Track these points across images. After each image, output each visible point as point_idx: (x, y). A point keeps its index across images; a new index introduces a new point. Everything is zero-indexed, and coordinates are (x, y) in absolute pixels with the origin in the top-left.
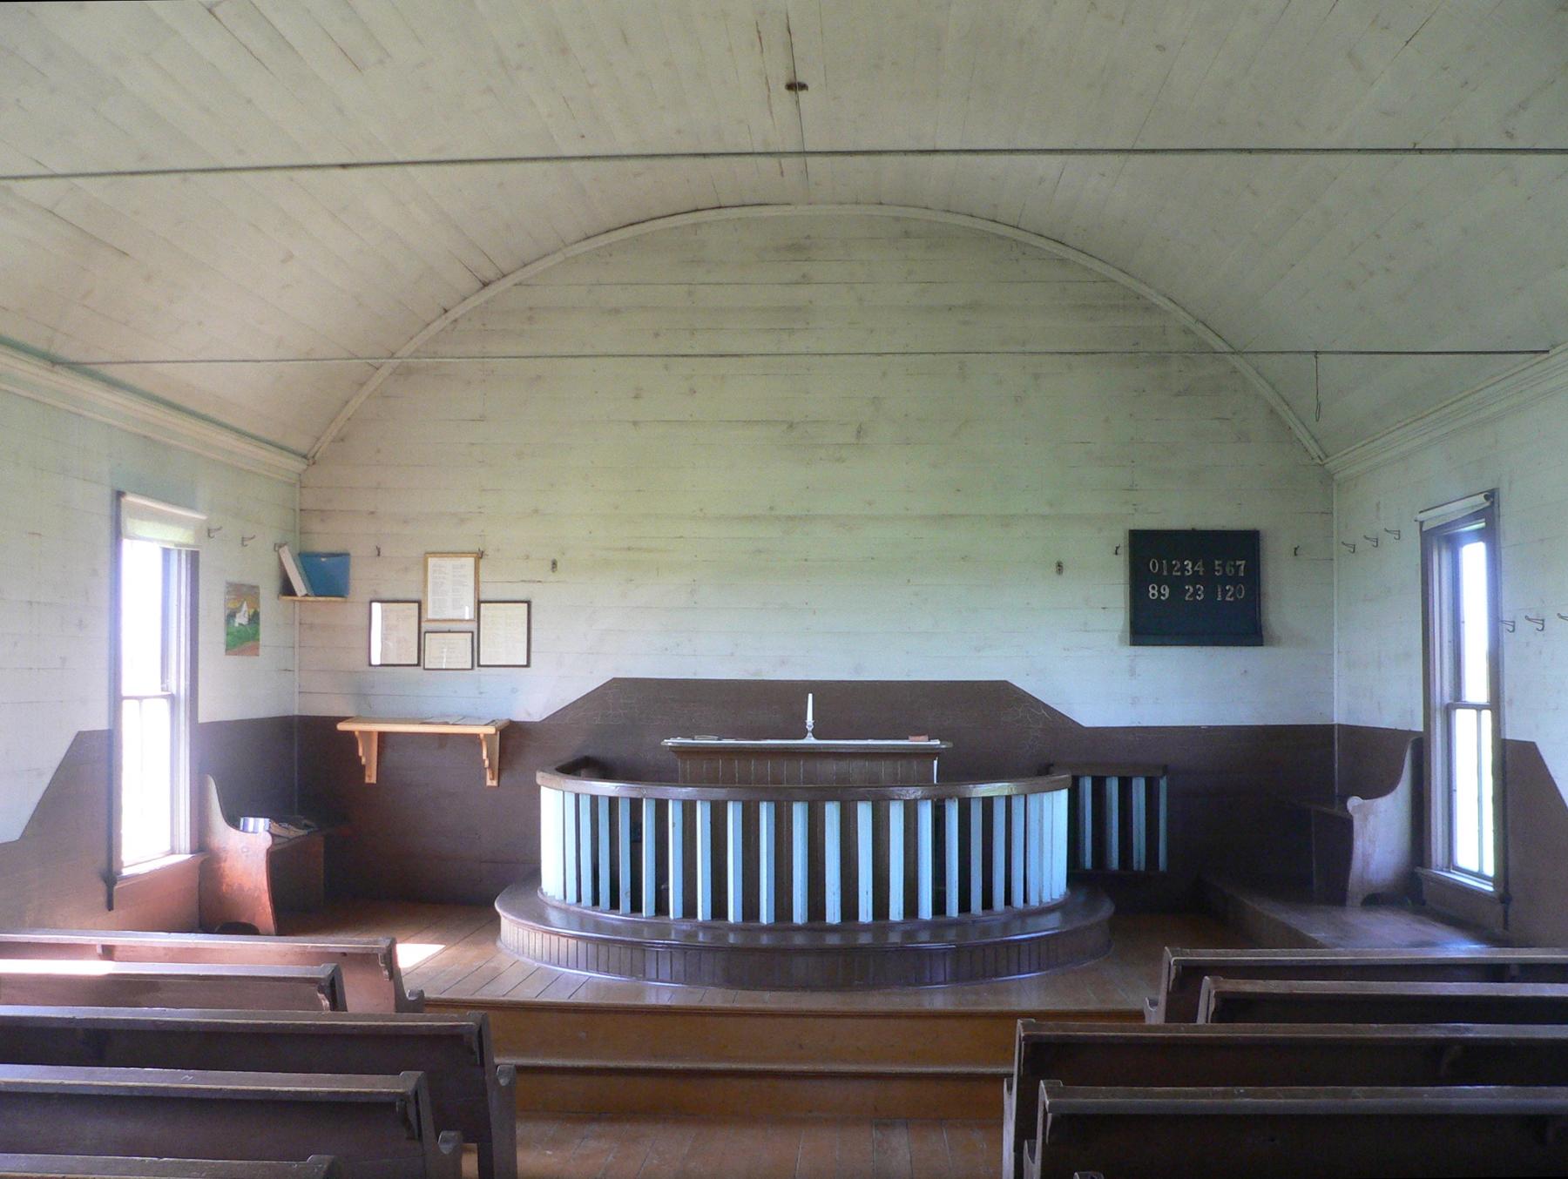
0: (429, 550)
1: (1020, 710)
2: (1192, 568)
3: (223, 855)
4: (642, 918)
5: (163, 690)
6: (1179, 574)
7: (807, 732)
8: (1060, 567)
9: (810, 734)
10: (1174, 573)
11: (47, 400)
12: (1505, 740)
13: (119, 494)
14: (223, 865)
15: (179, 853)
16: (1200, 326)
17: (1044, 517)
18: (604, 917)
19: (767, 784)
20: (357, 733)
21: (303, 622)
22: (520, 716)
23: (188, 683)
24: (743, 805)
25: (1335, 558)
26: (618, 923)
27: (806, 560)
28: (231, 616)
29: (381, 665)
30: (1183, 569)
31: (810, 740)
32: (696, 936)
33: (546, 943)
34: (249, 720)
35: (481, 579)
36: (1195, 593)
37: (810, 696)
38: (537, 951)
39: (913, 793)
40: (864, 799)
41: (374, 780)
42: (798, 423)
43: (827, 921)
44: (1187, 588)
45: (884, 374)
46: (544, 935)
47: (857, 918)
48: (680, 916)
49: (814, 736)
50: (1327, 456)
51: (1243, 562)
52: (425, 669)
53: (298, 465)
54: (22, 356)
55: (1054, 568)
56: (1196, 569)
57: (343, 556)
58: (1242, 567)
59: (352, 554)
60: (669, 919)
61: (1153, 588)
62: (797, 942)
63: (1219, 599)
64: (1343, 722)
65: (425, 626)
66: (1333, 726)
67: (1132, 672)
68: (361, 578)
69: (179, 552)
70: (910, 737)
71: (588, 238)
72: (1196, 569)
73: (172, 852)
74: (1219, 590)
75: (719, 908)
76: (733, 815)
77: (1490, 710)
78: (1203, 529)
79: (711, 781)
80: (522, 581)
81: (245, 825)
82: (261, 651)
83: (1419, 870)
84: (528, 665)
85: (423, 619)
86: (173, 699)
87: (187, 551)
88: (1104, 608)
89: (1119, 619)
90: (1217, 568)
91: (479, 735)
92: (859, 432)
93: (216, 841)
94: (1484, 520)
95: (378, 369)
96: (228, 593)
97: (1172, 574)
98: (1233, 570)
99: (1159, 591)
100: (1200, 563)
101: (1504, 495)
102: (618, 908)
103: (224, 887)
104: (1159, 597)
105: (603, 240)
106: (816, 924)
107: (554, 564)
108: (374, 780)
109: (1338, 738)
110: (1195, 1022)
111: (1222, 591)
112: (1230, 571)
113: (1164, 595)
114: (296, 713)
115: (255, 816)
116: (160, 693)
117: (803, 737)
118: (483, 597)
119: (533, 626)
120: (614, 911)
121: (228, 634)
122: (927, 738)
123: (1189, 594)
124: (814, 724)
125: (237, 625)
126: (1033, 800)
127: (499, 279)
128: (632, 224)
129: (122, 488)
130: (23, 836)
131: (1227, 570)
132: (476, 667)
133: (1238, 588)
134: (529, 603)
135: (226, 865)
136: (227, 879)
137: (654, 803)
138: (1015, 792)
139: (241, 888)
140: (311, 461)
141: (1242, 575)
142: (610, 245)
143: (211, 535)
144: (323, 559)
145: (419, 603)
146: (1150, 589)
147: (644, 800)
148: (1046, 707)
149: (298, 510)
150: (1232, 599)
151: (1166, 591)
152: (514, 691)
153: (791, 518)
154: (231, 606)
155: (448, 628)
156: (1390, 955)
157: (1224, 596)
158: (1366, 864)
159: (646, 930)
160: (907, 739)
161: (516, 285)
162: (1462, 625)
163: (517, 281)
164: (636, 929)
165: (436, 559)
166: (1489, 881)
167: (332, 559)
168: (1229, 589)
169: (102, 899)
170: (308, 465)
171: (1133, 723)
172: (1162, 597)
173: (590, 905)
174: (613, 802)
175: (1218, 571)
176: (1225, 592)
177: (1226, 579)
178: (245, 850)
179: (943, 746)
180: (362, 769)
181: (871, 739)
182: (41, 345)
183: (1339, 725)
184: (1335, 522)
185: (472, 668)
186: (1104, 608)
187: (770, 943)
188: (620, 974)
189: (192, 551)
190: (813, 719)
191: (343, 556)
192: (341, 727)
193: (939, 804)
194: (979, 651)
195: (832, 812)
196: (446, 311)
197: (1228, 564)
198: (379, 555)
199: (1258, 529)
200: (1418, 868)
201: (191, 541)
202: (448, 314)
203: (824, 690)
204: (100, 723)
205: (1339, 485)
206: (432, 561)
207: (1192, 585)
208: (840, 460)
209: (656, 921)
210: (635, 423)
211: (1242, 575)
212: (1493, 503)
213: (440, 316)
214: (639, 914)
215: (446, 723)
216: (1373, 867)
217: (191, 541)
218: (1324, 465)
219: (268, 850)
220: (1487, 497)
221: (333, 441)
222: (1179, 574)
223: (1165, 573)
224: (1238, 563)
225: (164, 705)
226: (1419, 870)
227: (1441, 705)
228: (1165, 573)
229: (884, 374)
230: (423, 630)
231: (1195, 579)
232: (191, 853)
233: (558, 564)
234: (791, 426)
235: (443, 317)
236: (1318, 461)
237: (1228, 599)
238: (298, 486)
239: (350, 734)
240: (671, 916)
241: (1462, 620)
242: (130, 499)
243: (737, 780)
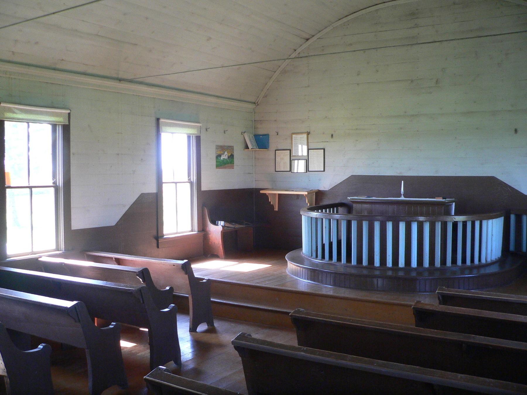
0: (293, 132)
3: (209, 233)
5: (189, 180)
8: (516, 131)
11: (123, 92)
13: (158, 120)
14: (209, 235)
15: (195, 232)
17: (509, 111)
18: (314, 261)
20: (267, 194)
21: (256, 157)
22: (322, 189)
23: (196, 178)
26: (317, 262)
28: (219, 156)
29: (297, 173)
31: (402, 198)
33: (292, 266)
35: (309, 142)
37: (403, 182)
39: (421, 219)
40: (377, 220)
41: (277, 210)
42: (415, 80)
43: (387, 266)
45: (446, 59)
49: (404, 197)
52: (292, 172)
53: (252, 106)
54: (106, 79)
55: (513, 131)
57: (267, 135)
59: (270, 135)
62: (399, 274)
65: (292, 158)
68: (273, 143)
69: (193, 136)
70: (436, 198)
71: (340, 19)
73: (192, 231)
80: (322, 142)
81: (218, 223)
82: (235, 167)
84: (324, 171)
85: (291, 156)
86: (191, 183)
87: (195, 136)
91: (303, 195)
92: (437, 82)
93: (207, 229)
95: (275, 72)
96: (217, 149)
103: (210, 243)
105: (345, 20)
107: (332, 135)
108: (277, 210)
110: (187, 298)
114: (254, 187)
115: (220, 220)
116: (188, 181)
117: (400, 196)
118: (310, 148)
119: (326, 157)
121: (216, 162)
122: (442, 198)
124: (404, 192)
125: (222, 159)
126: (484, 223)
127: (311, 37)
128: (354, 13)
129: (158, 117)
130: (117, 224)
132: (308, 172)
134: (324, 149)
135: (210, 236)
136: (211, 240)
138: (424, 220)
139: (214, 243)
140: (257, 104)
142: (348, 21)
143: (207, 130)
144: (261, 137)
145: (290, 150)
147: (332, 219)
148: (510, 187)
149: (253, 121)
152: (320, 180)
153: (412, 116)
154: (219, 153)
155: (299, 158)
160: (435, 198)
161: (317, 39)
163: (318, 37)
164: (323, 265)
165: (295, 135)
167: (263, 136)
169: (155, 245)
170: (256, 106)
174: (316, 219)
178: (215, 231)
180: (272, 207)
181: (390, 197)
182: (115, 76)
185: (306, 172)
188: (308, 279)
189: (196, 136)
190: (404, 190)
191: (267, 135)
192: (261, 192)
193: (465, 223)
195: (390, 226)
196: (295, 50)
198: (278, 134)
201: (196, 132)
202: (296, 51)
203: (409, 180)
204: (153, 190)
206: (294, 136)
208: (430, 93)
210: (358, 84)
213: (294, 52)
215: (293, 191)
217: (196, 132)
219: (221, 232)
221: (263, 97)
225: (188, 185)
229: (446, 59)
230: (291, 159)
232: (198, 232)
233: (334, 136)
234: (412, 81)
235: (295, 52)
238: (253, 113)
239: (265, 194)
240: (333, 262)
242: (162, 120)
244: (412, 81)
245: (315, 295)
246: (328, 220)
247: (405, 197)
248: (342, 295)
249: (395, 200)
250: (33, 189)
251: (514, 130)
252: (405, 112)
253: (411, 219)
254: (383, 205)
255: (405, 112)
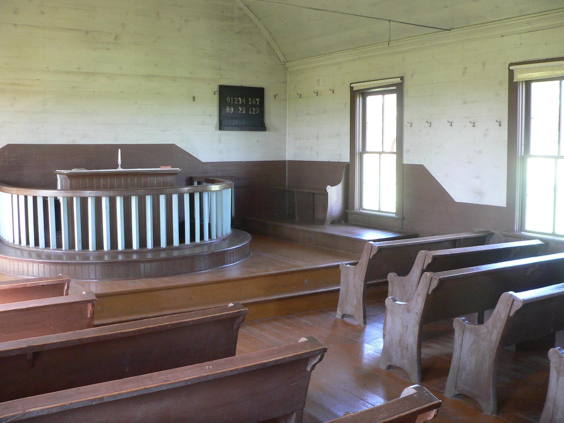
1: (179, 156)
2: (241, 101)
4: (62, 251)
6: (237, 103)
7: (118, 165)
9: (120, 166)
10: (235, 103)
12: (404, 164)
16: (246, 8)
17: (189, 78)
19: (160, 186)
24: (138, 197)
25: (288, 99)
27: (94, 92)
30: (238, 101)
31: (120, 169)
32: (117, 257)
34: (247, 162)
36: (242, 111)
37: (120, 150)
38: (34, 272)
43: (161, 246)
44: (239, 108)
45: (127, 14)
46: (40, 264)
47: (173, 244)
48: (81, 249)
50: (287, 62)
51: (259, 99)
55: (192, 99)
56: (243, 101)
58: (258, 101)
60: (89, 251)
61: (228, 108)
63: (250, 113)
64: (289, 159)
66: (286, 161)
67: (220, 141)
72: (243, 101)
74: (250, 109)
75: (99, 244)
76: (105, 202)
77: (396, 154)
78: (245, 86)
79: (105, 188)
83: (347, 211)
88: (210, 115)
89: (215, 120)
90: (250, 101)
94: (396, 87)
97: (234, 103)
98: (255, 103)
99: (230, 109)
100: (244, 99)
101: (405, 79)
102: (50, 246)
104: (230, 112)
106: (143, 250)
109: (288, 164)
111: (251, 110)
112: (254, 102)
113: (232, 111)
117: (117, 167)
120: (47, 248)
123: (240, 111)
131: (253, 102)
133: (257, 109)
137: (79, 198)
141: (258, 104)
146: (227, 108)
150: (254, 113)
151: (232, 109)
153: (87, 73)
156: (379, 243)
157: (252, 112)
158: (331, 210)
159: (77, 257)
162: (366, 124)
166: (394, 214)
168: (254, 110)
171: (220, 160)
172: (231, 112)
173: (56, 248)
175: (250, 102)
176: (252, 111)
177: (253, 106)
179: (180, 170)
183: (288, 161)
184: (288, 86)
186: (210, 115)
187: (123, 259)
190: (121, 160)
194: (164, 132)
197: (253, 100)
199: (263, 87)
200: (347, 210)
205: (289, 72)
207: (241, 107)
208: (108, 49)
209: (82, 252)
211: (258, 104)
212: (402, 81)
214: (60, 249)
216: (334, 211)
218: (284, 65)
220: (401, 79)
222: (237, 103)
223: (232, 102)
224: (257, 100)
226: (347, 211)
227: (358, 153)
228: (232, 102)
229: (127, 14)
231: (242, 105)
234: (87, 32)
236: (284, 63)
237: (253, 113)
241: (366, 122)
243: (143, 186)
244: (87, 32)
245: (135, 292)
246: (79, 198)
247: (122, 167)
248: (118, 290)
249: (125, 172)
250: (556, 154)
251: (192, 98)
252: (79, 69)
253: (19, 193)
254: (155, 177)
255: (79, 69)
